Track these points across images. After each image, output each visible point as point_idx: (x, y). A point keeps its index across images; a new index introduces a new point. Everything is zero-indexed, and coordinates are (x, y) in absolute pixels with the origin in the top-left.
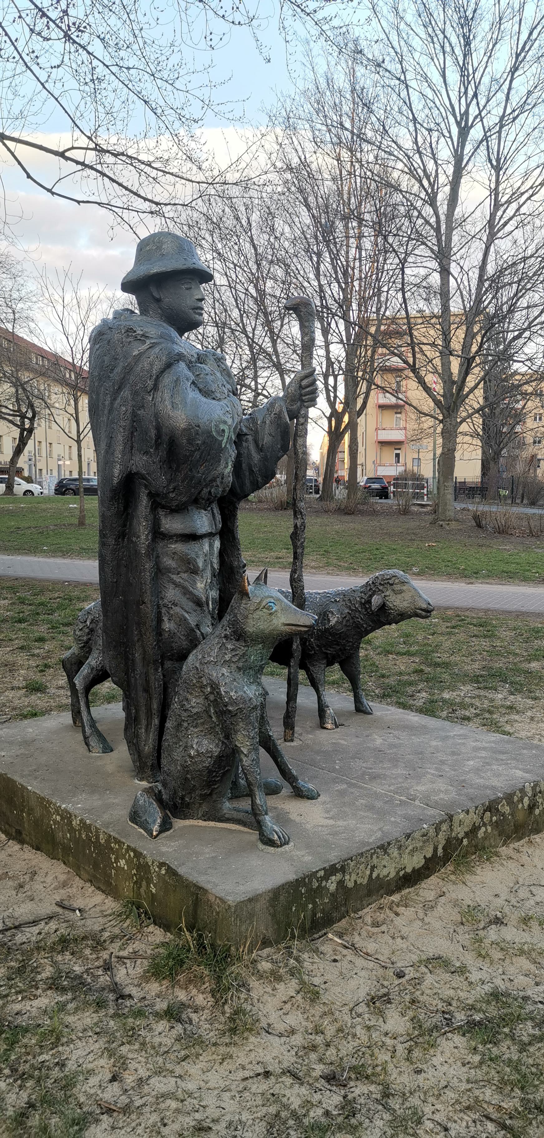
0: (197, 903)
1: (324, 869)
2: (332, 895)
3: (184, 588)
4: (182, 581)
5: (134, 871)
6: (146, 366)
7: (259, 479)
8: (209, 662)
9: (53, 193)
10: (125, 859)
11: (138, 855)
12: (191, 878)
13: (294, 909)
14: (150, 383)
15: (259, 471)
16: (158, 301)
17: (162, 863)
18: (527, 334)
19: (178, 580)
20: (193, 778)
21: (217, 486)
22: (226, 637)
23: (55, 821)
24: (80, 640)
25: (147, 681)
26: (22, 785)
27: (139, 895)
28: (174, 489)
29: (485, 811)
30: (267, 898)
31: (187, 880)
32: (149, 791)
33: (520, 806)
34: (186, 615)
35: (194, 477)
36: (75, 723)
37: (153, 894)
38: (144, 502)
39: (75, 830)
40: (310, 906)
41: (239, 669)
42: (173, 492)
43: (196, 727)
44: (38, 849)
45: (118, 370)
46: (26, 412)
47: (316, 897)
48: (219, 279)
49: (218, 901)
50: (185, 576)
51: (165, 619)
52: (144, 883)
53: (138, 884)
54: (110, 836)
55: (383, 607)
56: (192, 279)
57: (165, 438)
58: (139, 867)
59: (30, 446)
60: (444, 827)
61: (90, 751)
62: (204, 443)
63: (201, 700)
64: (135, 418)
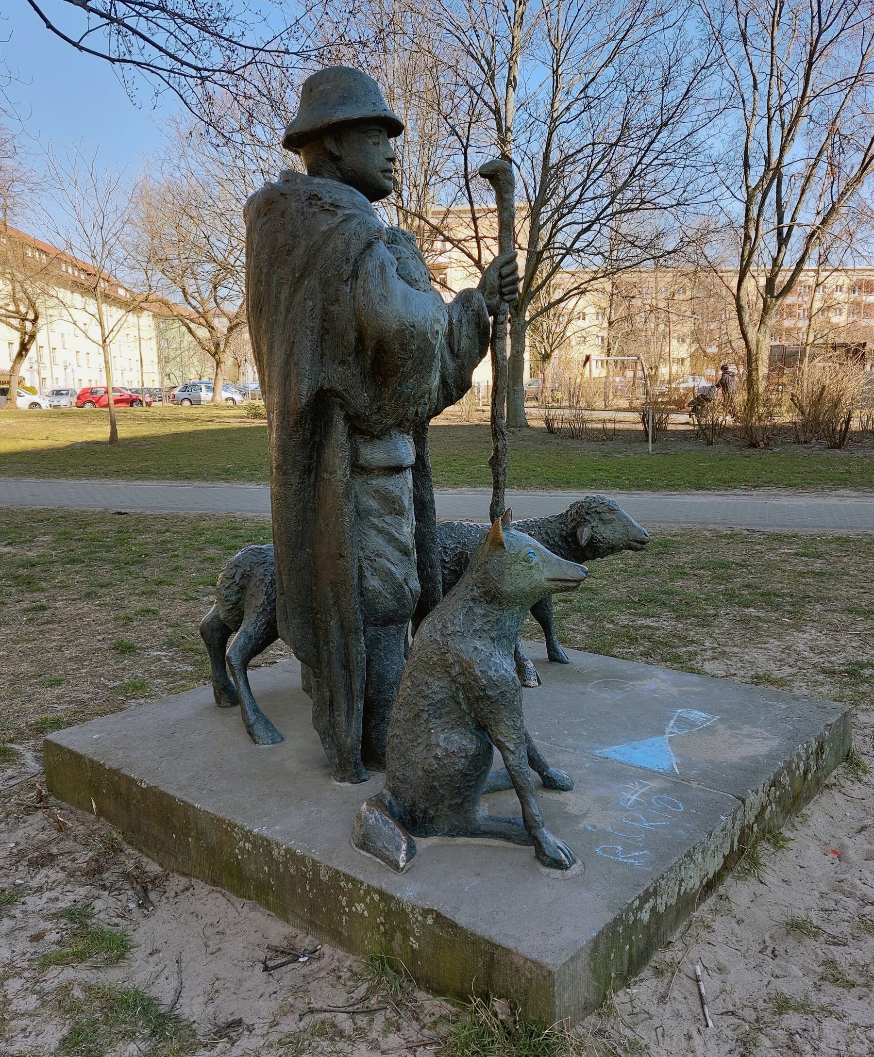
0: (491, 965)
1: (639, 897)
2: (647, 927)
3: (389, 534)
4: (385, 526)
5: (381, 919)
6: (341, 247)
7: (454, 393)
8: (454, 633)
9: (81, 48)
10: (364, 902)
11: (386, 897)
12: (479, 932)
13: (612, 956)
14: (347, 269)
15: (454, 382)
16: (336, 159)
17: (428, 910)
18: (596, 227)
19: (380, 525)
20: (441, 786)
21: (425, 404)
22: (473, 600)
23: (243, 851)
24: (227, 601)
25: (347, 655)
26: (185, 802)
27: (389, 950)
28: (379, 409)
29: (771, 786)
30: (588, 951)
31: (472, 935)
32: (378, 802)
33: (797, 773)
34: (393, 569)
35: (403, 392)
36: (218, 701)
37: (413, 951)
38: (340, 428)
39: (278, 863)
40: (627, 947)
41: (493, 639)
42: (376, 413)
43: (440, 718)
44: (215, 883)
45: (301, 250)
46: (27, 313)
47: (631, 935)
48: (411, 133)
49: (529, 964)
50: (387, 518)
51: (367, 574)
52: (398, 935)
53: (389, 935)
54: (338, 872)
55: (592, 541)
56: (380, 131)
57: (371, 344)
58: (388, 915)
59: (33, 349)
60: (739, 815)
61: (255, 743)
62: (418, 348)
63: (444, 683)
64: (327, 317)
